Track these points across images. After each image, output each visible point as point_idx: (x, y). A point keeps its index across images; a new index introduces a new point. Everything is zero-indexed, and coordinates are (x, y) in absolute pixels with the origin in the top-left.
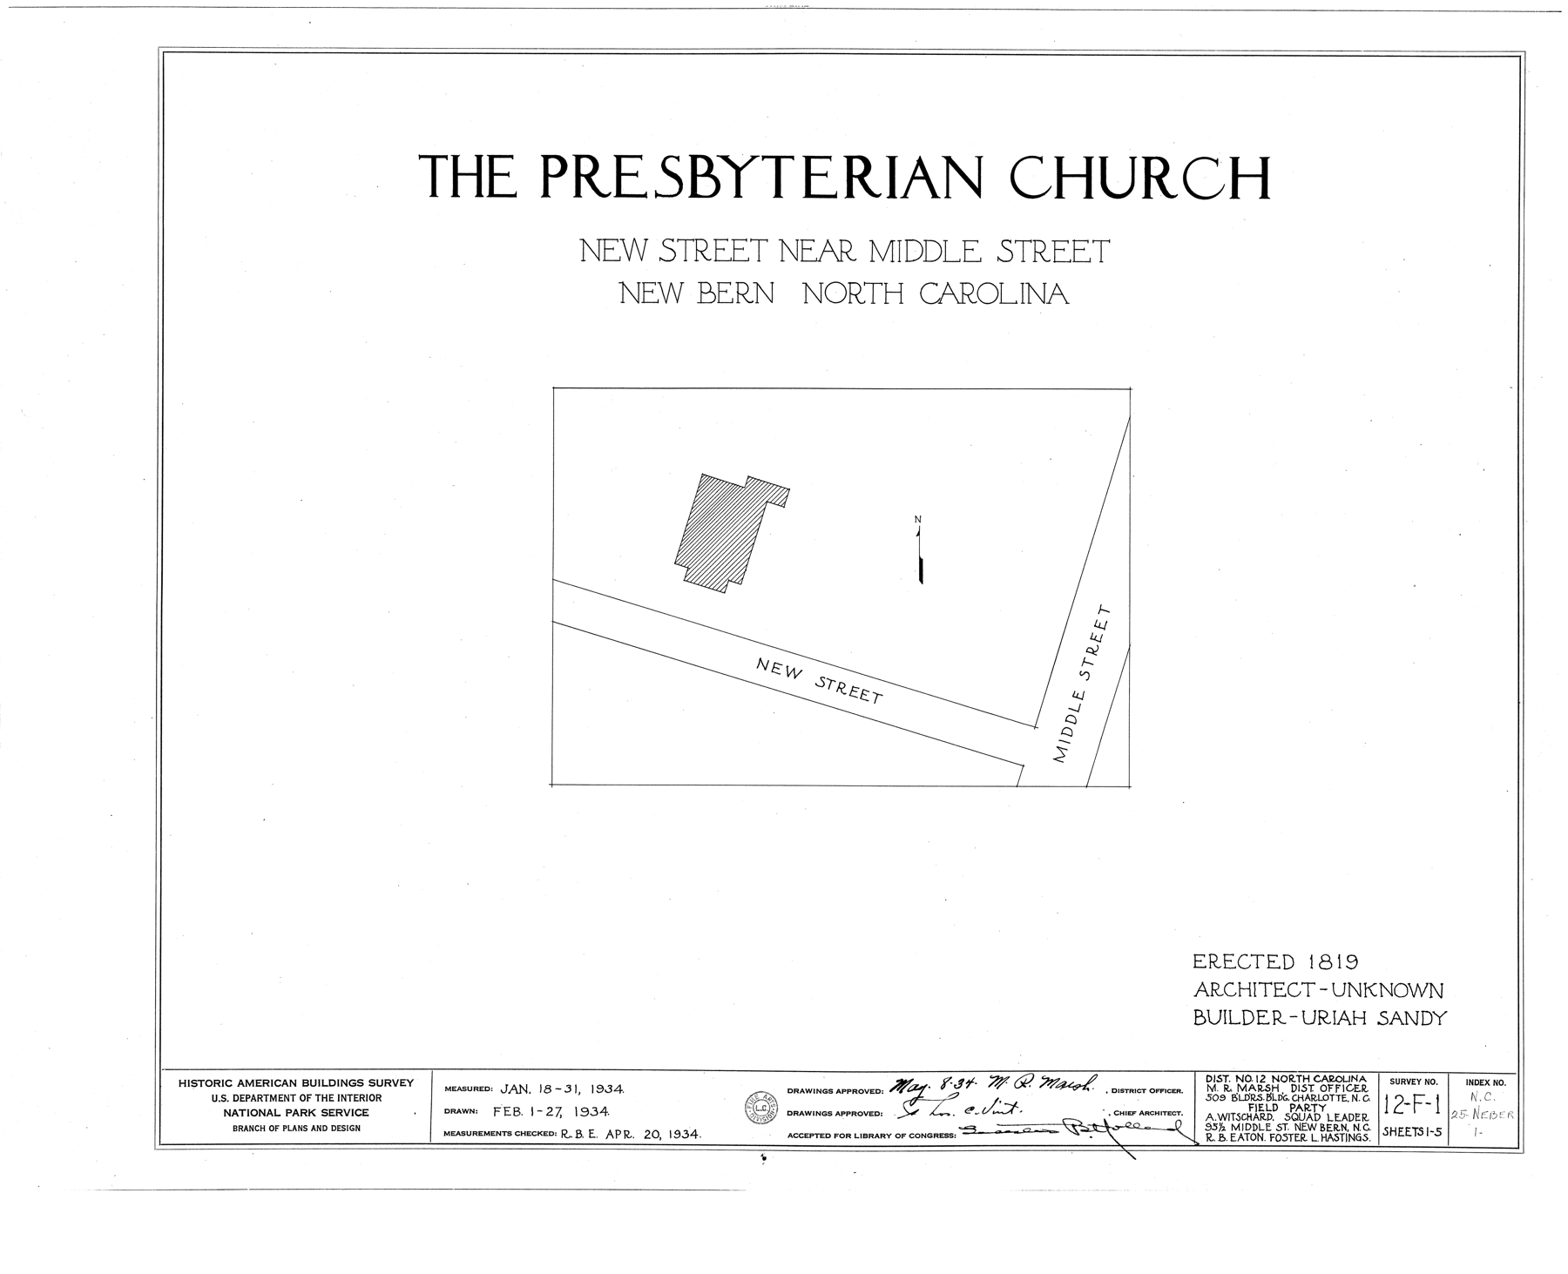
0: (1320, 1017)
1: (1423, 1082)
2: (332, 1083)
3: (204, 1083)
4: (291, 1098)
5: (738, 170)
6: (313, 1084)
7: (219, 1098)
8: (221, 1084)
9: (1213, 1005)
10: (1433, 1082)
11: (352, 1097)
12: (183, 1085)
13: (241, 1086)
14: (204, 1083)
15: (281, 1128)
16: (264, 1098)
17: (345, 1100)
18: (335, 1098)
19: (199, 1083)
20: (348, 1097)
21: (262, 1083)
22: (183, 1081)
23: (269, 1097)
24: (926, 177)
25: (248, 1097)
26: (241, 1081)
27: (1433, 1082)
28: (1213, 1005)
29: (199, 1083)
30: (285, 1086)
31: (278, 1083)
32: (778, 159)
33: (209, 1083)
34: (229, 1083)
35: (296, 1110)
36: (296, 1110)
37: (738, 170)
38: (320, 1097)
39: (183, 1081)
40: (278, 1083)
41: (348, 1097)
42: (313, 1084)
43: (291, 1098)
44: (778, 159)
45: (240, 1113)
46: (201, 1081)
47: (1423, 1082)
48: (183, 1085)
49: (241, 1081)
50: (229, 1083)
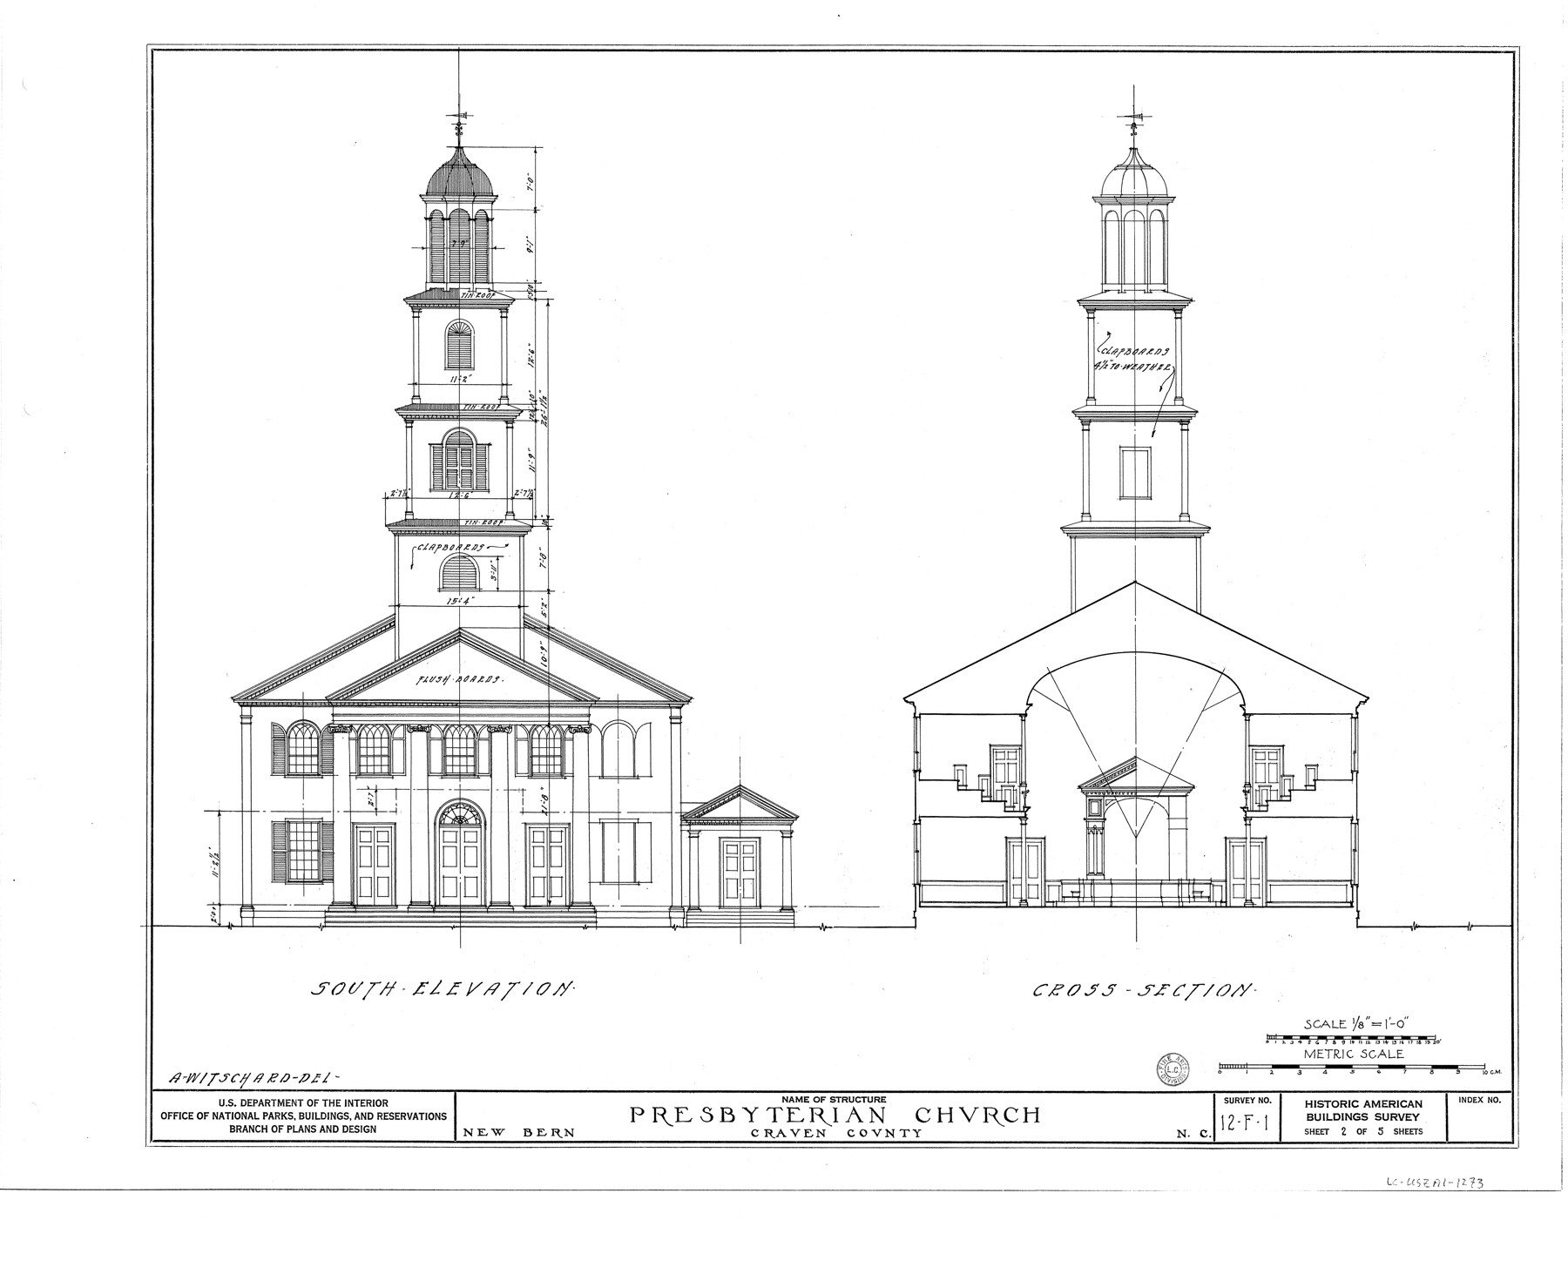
0: (535, 727)
1: (1256, 1100)
2: (1337, 1117)
3: (1330, 1104)
4: (298, 1103)
5: (751, 1114)
6: (1318, 1118)
7: (227, 1103)
8: (1396, 1105)
9: (1316, 1111)
10: (1266, 1100)
11: (359, 1102)
12: (1309, 1106)
13: (1367, 1107)
14: (1330, 1104)
15: (210, 1115)
16: (271, 1103)
17: (352, 1105)
18: (342, 1103)
19: (1325, 1104)
20: (355, 1103)
21: (1388, 1103)
22: (1309, 1102)
23: (276, 1102)
24: (856, 1113)
25: (255, 1101)
26: (1367, 1101)
27: (1496, 1100)
28: (1316, 1111)
29: (1325, 1104)
30: (1411, 1107)
31: (1404, 1104)
32: (775, 1109)
33: (1335, 1104)
34: (1355, 1104)
35: (1411, 1101)
36: (1411, 1101)
37: (751, 1114)
38: (328, 1102)
39: (1309, 1102)
40: (1404, 1104)
41: (355, 1103)
42: (1318, 1118)
43: (298, 1103)
44: (775, 1109)
45: (225, 1116)
46: (1328, 1102)
47: (1256, 1100)
48: (1309, 1106)
49: (1367, 1101)
50: (1355, 1104)
